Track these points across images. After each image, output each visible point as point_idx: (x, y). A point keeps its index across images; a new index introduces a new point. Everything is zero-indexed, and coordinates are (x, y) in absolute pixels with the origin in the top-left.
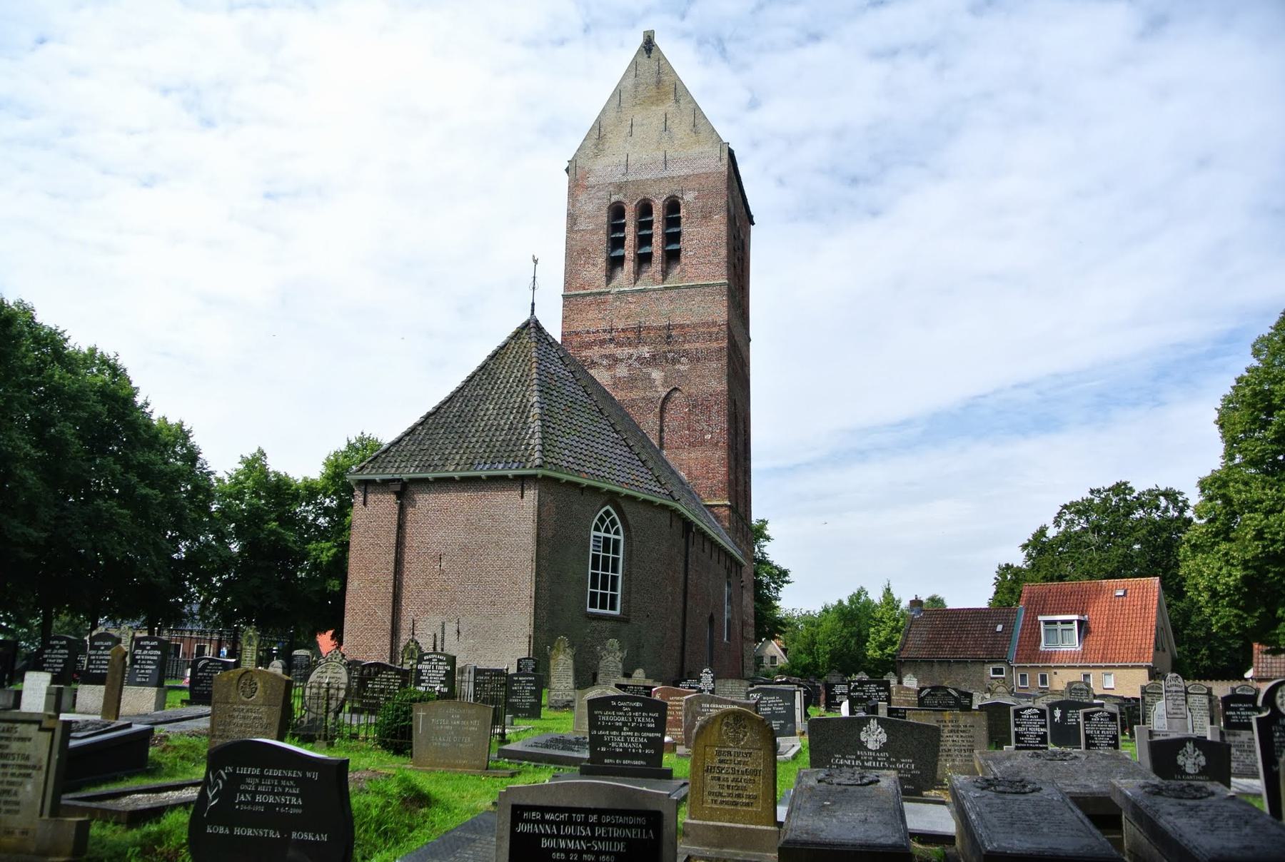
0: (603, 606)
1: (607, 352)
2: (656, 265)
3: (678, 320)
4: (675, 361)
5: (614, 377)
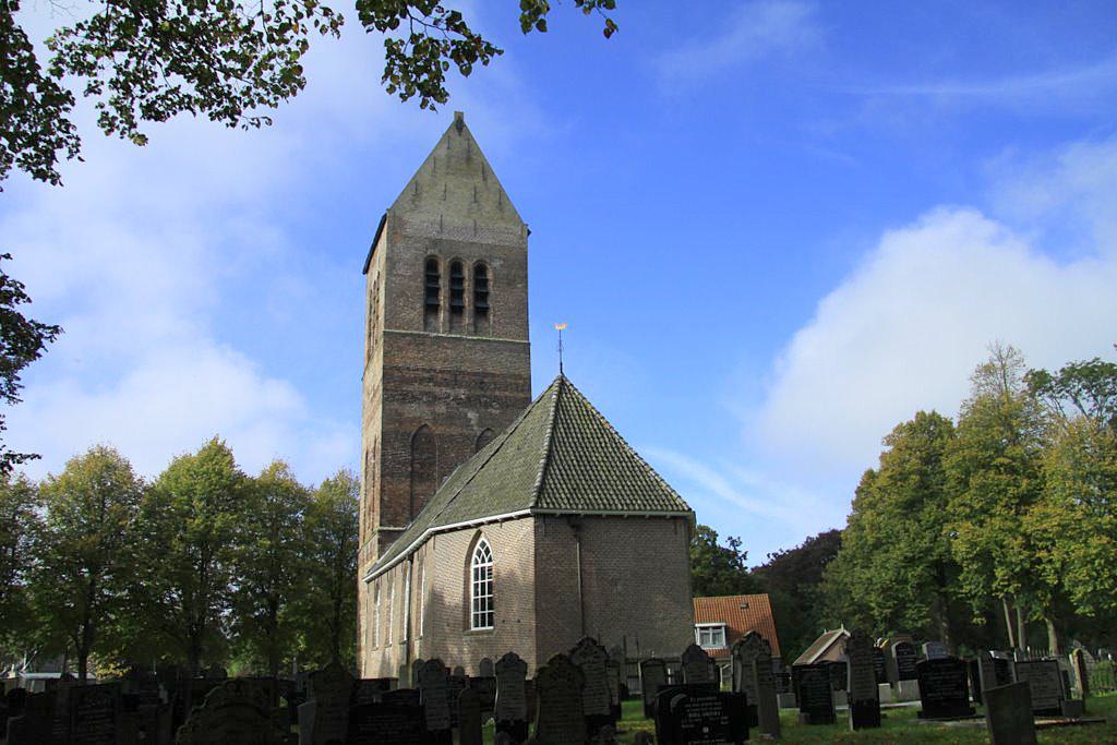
0: (483, 625)
1: (427, 389)
3: (490, 370)
4: (487, 405)
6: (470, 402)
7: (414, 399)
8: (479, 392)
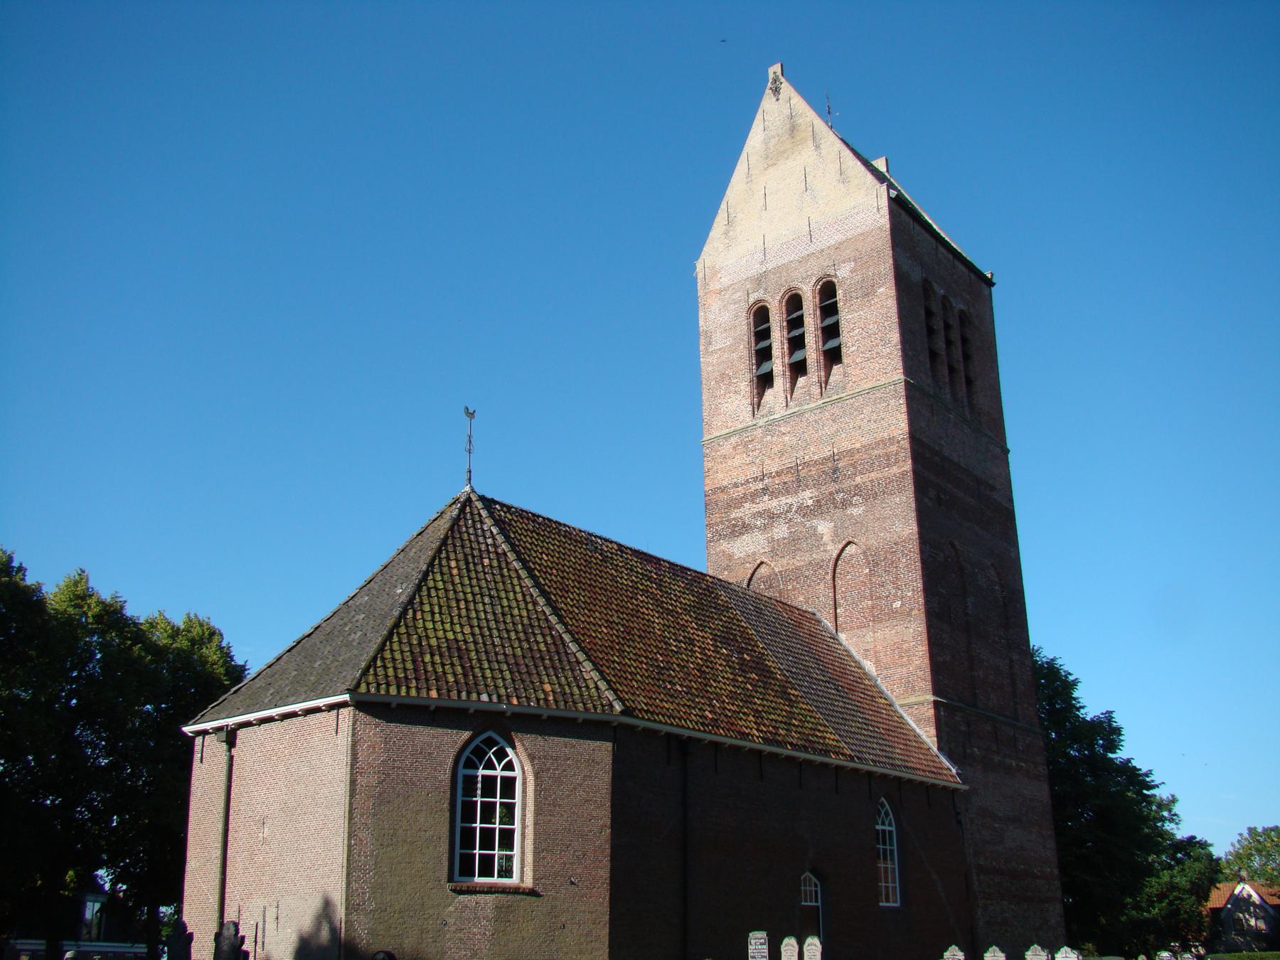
1: (761, 507)
2: (780, 383)
4: (845, 504)
5: (771, 541)
6: (818, 509)
7: (745, 528)
8: (833, 487)
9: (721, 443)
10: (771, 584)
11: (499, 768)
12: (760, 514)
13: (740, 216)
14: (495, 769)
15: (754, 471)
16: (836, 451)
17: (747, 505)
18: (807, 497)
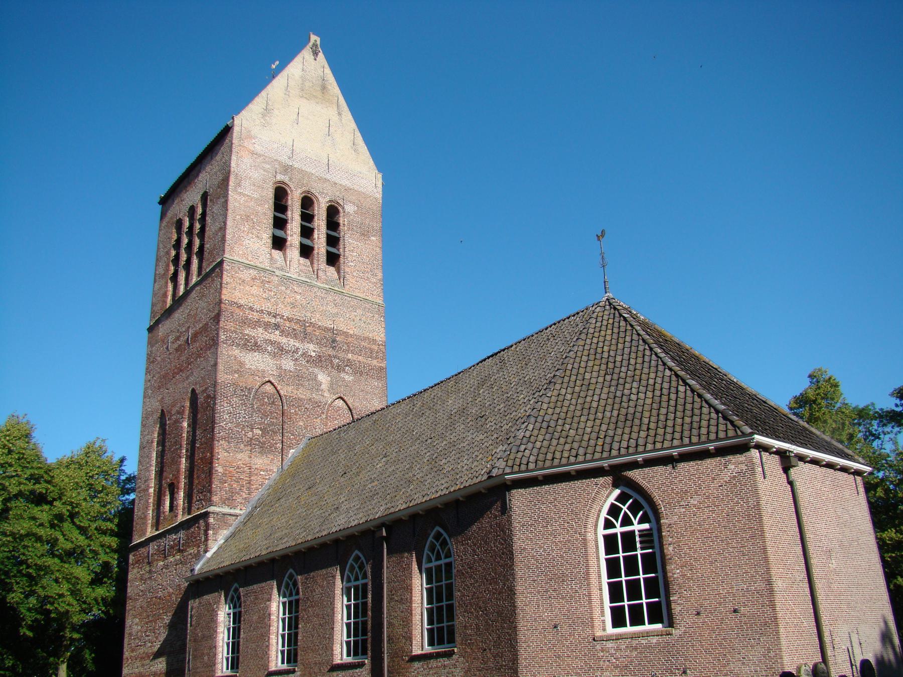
1: (272, 337)
4: (339, 369)
9: (241, 269)
10: (273, 402)
11: (618, 525)
12: (272, 343)
13: (276, 112)
14: (633, 524)
15: (267, 306)
16: (335, 328)
17: (261, 330)
18: (312, 349)
